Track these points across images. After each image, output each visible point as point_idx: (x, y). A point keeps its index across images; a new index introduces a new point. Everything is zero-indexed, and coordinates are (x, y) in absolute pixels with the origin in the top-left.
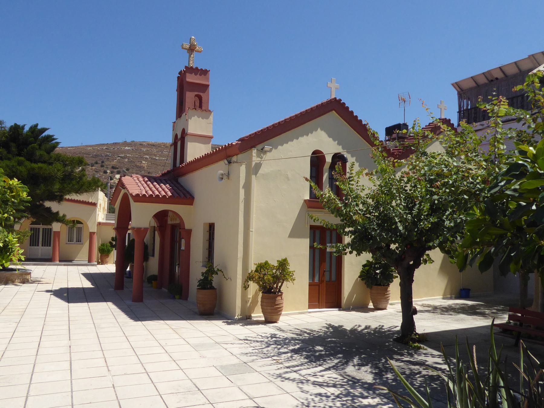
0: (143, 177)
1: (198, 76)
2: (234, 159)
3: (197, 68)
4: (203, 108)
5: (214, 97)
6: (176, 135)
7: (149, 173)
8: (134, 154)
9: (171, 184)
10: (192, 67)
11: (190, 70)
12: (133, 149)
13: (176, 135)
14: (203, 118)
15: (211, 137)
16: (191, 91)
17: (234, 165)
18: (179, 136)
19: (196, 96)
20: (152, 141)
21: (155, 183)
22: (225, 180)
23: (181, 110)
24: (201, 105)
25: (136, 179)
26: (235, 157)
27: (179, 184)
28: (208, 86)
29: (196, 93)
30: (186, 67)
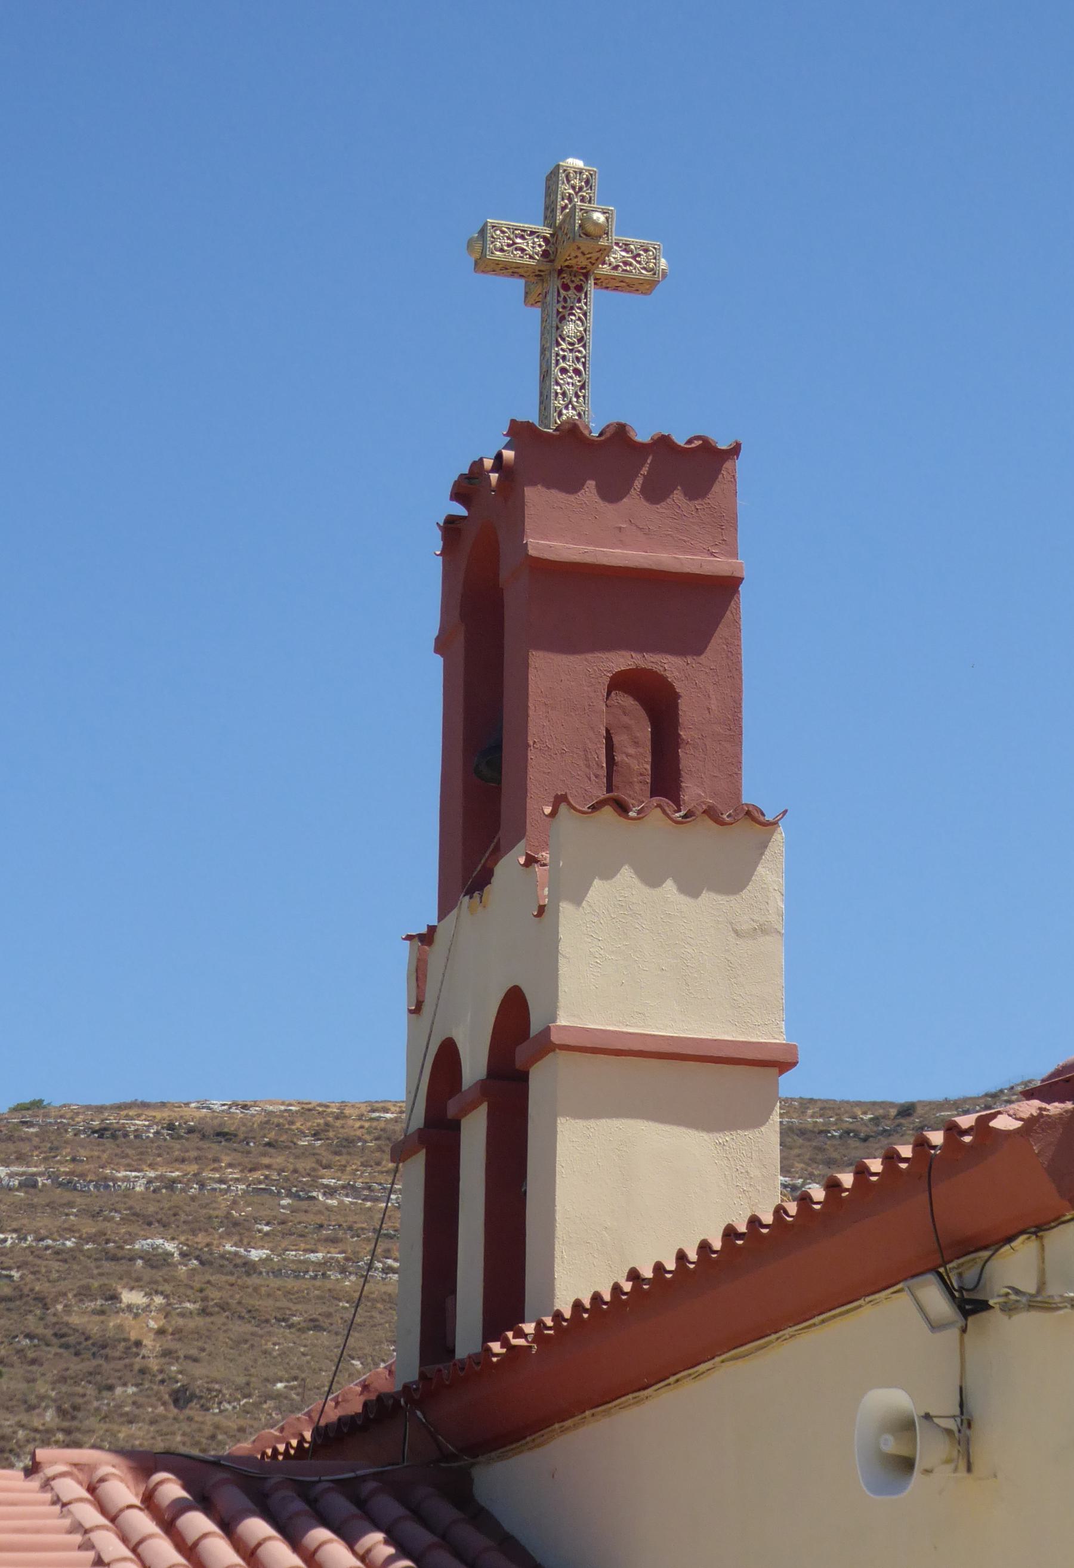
0: (144, 1464)
1: (634, 501)
2: (1015, 1266)
3: (619, 434)
4: (692, 791)
5: (785, 690)
6: (447, 1057)
7: (181, 1398)
8: (43, 1222)
9: (414, 1530)
10: (572, 432)
11: (554, 453)
12: (29, 1184)
13: (447, 1057)
14: (691, 890)
15: (780, 1063)
16: (573, 647)
17: (1010, 1333)
18: (474, 1066)
19: (621, 683)
20: (209, 1087)
21: (256, 1527)
22: (935, 1479)
23: (482, 817)
24: (668, 769)
25: (71, 1488)
26: (1023, 1249)
27: (480, 1517)
28: (725, 588)
29: (622, 661)
30: (519, 432)
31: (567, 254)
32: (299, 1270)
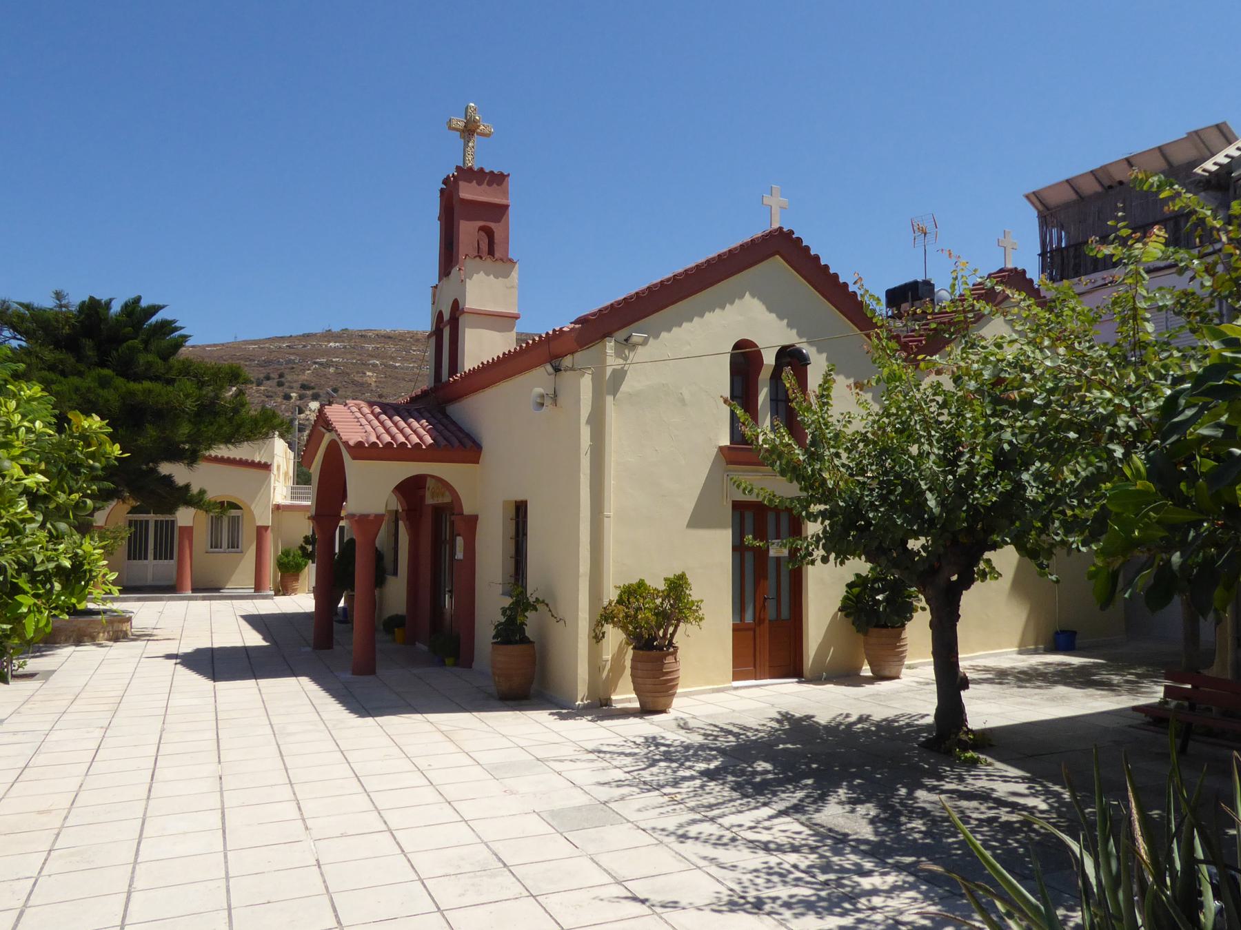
0: (371, 404)
1: (485, 186)
2: (567, 361)
3: (482, 170)
4: (497, 255)
5: (519, 232)
6: (440, 315)
9: (432, 420)
10: (471, 169)
11: (466, 174)
13: (440, 315)
14: (496, 277)
15: (516, 317)
16: (470, 219)
17: (566, 376)
18: (446, 316)
19: (482, 229)
20: (387, 328)
21: (397, 418)
23: (449, 259)
24: (492, 249)
25: (355, 409)
26: (569, 358)
27: (447, 417)
28: (506, 207)
29: (482, 223)
30: (458, 168)
31: (470, 126)
32: (407, 368)
